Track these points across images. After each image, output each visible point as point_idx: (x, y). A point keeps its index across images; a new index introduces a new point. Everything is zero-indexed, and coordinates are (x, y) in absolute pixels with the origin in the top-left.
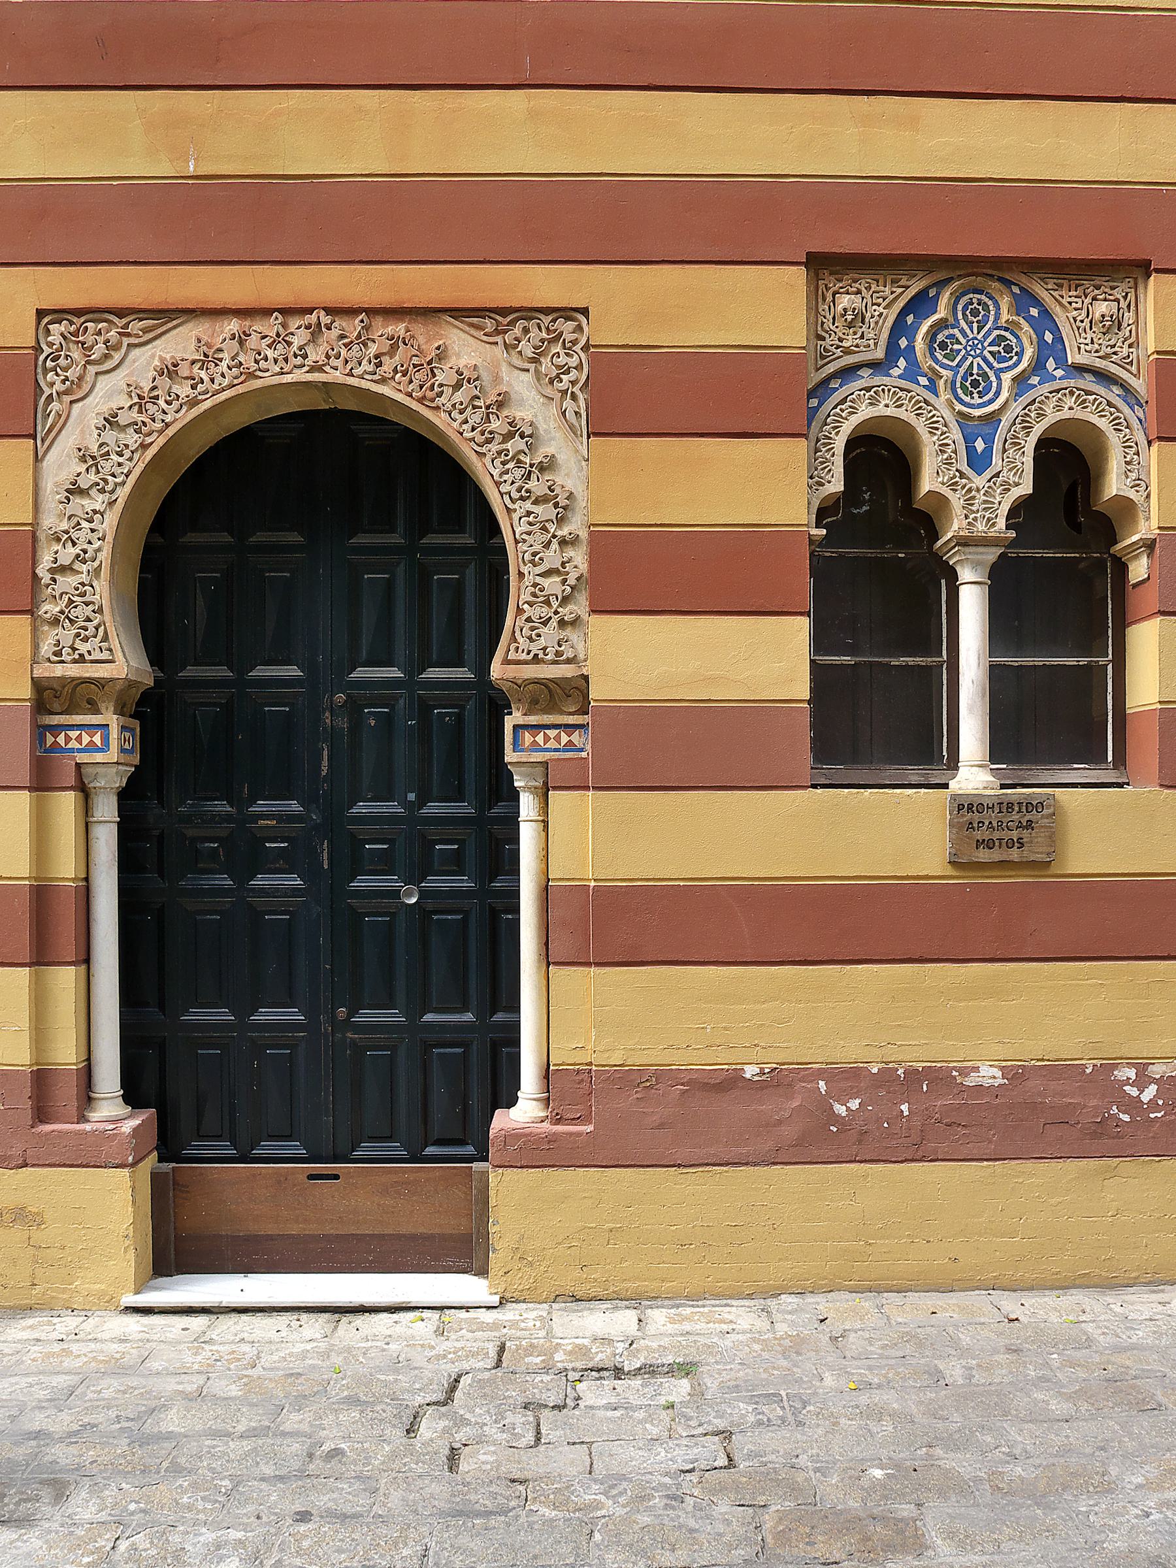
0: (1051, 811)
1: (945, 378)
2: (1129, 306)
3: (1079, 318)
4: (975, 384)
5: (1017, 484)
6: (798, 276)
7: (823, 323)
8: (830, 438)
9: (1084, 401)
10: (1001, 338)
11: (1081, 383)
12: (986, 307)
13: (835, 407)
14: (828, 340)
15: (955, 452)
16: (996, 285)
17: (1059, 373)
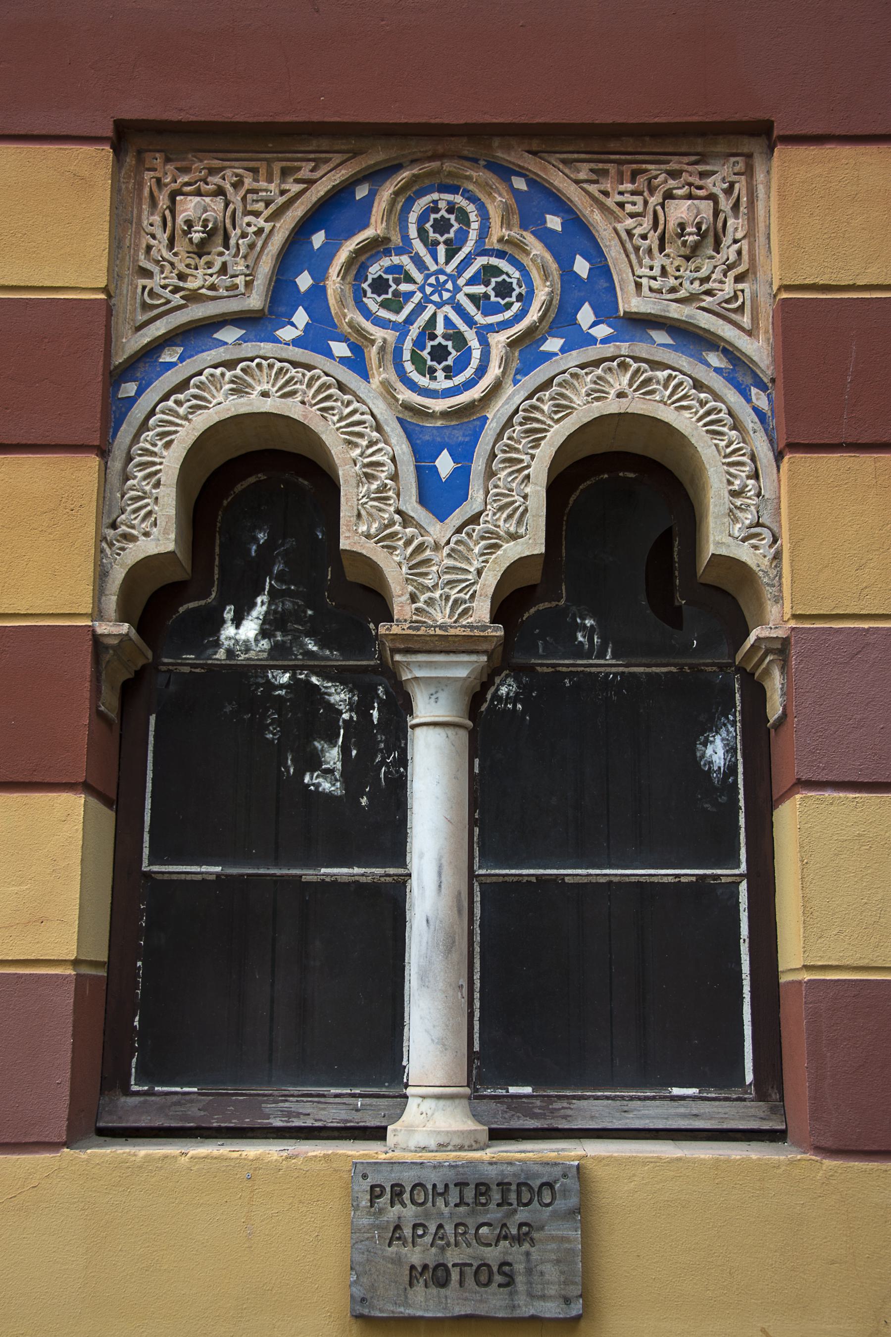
0: (573, 1201)
1: (379, 343)
2: (736, 206)
3: (637, 231)
4: (439, 353)
5: (514, 537)
6: (95, 162)
7: (149, 248)
8: (154, 454)
9: (648, 381)
10: (490, 271)
11: (642, 349)
12: (463, 217)
13: (166, 398)
14: (157, 277)
15: (394, 477)
16: (479, 174)
17: (602, 331)
